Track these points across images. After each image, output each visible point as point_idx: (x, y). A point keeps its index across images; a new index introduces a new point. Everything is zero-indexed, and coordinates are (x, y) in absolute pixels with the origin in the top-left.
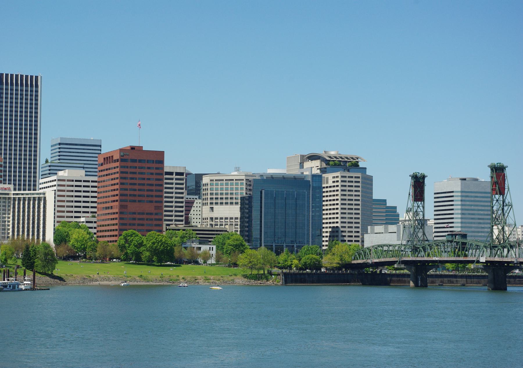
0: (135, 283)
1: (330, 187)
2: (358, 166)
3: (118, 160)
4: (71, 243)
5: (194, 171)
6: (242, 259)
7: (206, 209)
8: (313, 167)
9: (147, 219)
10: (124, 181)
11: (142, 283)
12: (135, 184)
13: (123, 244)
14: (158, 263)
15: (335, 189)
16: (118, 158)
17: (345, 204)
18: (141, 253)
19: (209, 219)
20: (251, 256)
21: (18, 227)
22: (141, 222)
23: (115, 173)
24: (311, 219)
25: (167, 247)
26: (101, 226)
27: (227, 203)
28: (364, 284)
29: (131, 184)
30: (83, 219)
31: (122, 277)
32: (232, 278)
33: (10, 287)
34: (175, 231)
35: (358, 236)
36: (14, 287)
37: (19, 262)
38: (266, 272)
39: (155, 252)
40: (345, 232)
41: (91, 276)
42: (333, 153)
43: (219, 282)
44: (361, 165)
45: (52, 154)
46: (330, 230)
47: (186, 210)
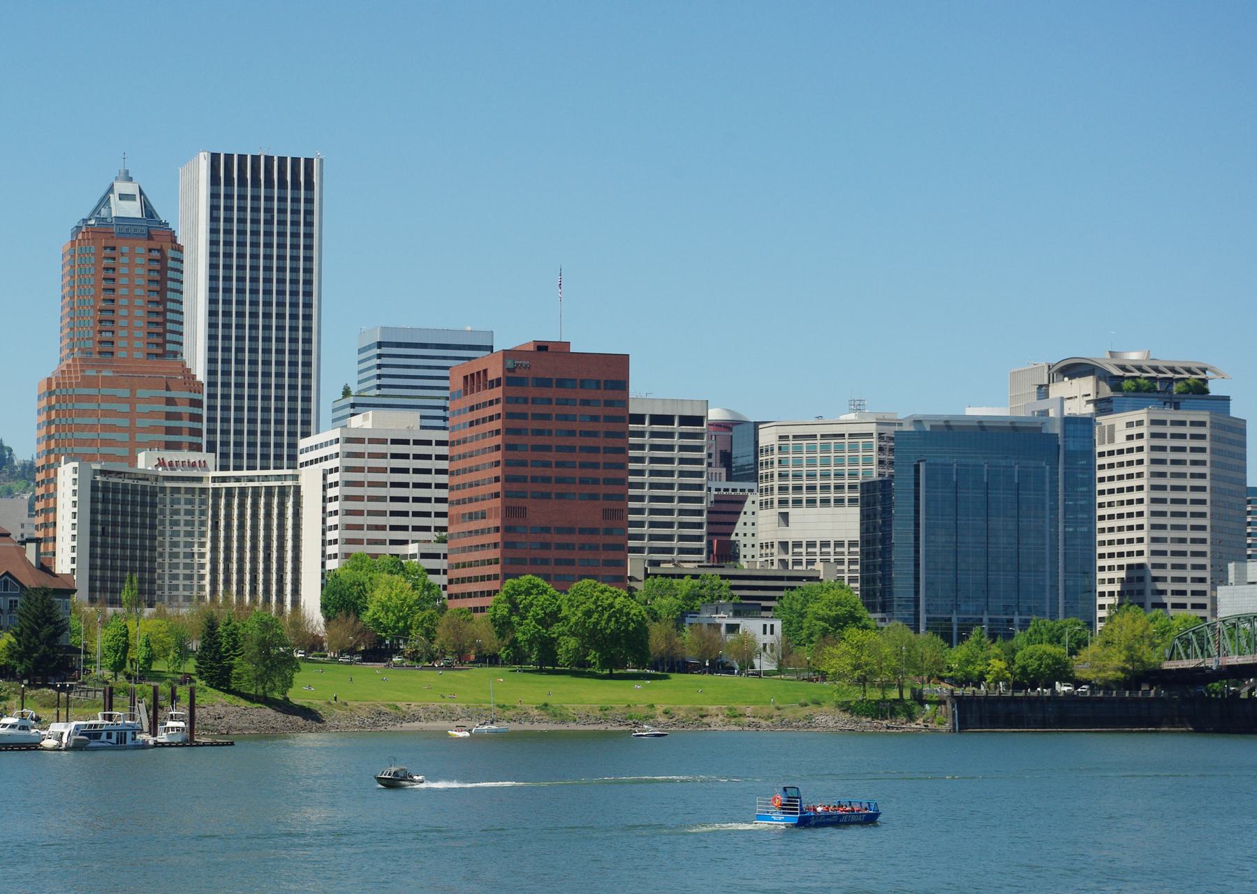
0: (526, 726)
1: (1121, 452)
2: (1207, 392)
3: (498, 382)
4: (369, 613)
5: (752, 418)
6: (838, 657)
7: (772, 514)
8: (1076, 397)
9: (582, 547)
10: (516, 440)
11: (544, 727)
12: (547, 448)
13: (503, 617)
14: (602, 667)
15: (1135, 457)
16: (500, 375)
17: (1163, 501)
18: (555, 639)
19: (776, 545)
20: (860, 647)
21: (227, 570)
22: (564, 554)
23: (491, 418)
24: (1061, 543)
25: (627, 624)
26: (458, 566)
27: (825, 502)
28: (1200, 729)
29: (535, 448)
30: (412, 549)
31: (490, 709)
32: (806, 711)
33: (109, 736)
34: (669, 580)
35: (1203, 593)
36: (122, 738)
37: (190, 666)
38: (907, 695)
39: (592, 637)
40: (1164, 579)
41: (399, 704)
42: (1134, 356)
43: (769, 722)
44: (1215, 389)
45: (360, 372)
46: (1123, 574)
47: (709, 523)
